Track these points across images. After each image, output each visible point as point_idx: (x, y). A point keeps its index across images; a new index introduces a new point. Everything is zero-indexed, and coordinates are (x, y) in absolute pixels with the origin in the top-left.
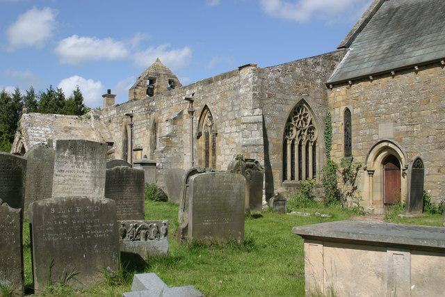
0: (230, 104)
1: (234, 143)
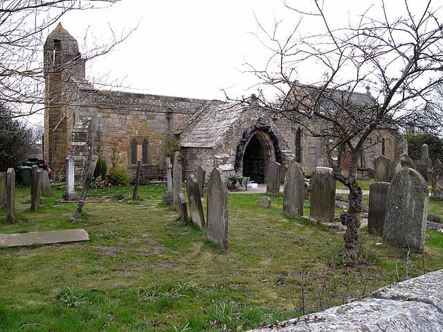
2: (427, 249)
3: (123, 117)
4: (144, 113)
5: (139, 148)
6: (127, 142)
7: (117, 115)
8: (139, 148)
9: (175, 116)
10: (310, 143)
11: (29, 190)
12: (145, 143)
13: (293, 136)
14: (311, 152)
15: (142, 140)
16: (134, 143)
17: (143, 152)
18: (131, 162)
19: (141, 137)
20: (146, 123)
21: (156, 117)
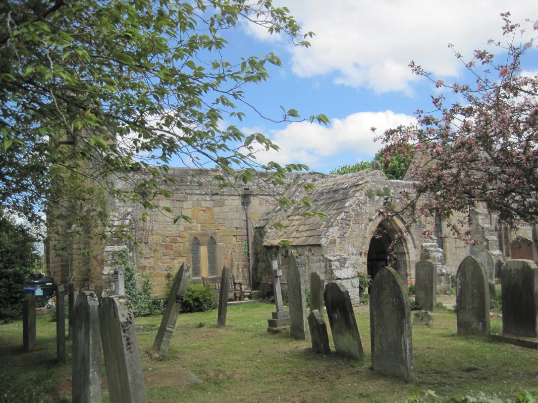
4: (208, 198)
5: (204, 251)
6: (185, 244)
8: (204, 251)
12: (212, 242)
16: (196, 243)
21: (226, 203)
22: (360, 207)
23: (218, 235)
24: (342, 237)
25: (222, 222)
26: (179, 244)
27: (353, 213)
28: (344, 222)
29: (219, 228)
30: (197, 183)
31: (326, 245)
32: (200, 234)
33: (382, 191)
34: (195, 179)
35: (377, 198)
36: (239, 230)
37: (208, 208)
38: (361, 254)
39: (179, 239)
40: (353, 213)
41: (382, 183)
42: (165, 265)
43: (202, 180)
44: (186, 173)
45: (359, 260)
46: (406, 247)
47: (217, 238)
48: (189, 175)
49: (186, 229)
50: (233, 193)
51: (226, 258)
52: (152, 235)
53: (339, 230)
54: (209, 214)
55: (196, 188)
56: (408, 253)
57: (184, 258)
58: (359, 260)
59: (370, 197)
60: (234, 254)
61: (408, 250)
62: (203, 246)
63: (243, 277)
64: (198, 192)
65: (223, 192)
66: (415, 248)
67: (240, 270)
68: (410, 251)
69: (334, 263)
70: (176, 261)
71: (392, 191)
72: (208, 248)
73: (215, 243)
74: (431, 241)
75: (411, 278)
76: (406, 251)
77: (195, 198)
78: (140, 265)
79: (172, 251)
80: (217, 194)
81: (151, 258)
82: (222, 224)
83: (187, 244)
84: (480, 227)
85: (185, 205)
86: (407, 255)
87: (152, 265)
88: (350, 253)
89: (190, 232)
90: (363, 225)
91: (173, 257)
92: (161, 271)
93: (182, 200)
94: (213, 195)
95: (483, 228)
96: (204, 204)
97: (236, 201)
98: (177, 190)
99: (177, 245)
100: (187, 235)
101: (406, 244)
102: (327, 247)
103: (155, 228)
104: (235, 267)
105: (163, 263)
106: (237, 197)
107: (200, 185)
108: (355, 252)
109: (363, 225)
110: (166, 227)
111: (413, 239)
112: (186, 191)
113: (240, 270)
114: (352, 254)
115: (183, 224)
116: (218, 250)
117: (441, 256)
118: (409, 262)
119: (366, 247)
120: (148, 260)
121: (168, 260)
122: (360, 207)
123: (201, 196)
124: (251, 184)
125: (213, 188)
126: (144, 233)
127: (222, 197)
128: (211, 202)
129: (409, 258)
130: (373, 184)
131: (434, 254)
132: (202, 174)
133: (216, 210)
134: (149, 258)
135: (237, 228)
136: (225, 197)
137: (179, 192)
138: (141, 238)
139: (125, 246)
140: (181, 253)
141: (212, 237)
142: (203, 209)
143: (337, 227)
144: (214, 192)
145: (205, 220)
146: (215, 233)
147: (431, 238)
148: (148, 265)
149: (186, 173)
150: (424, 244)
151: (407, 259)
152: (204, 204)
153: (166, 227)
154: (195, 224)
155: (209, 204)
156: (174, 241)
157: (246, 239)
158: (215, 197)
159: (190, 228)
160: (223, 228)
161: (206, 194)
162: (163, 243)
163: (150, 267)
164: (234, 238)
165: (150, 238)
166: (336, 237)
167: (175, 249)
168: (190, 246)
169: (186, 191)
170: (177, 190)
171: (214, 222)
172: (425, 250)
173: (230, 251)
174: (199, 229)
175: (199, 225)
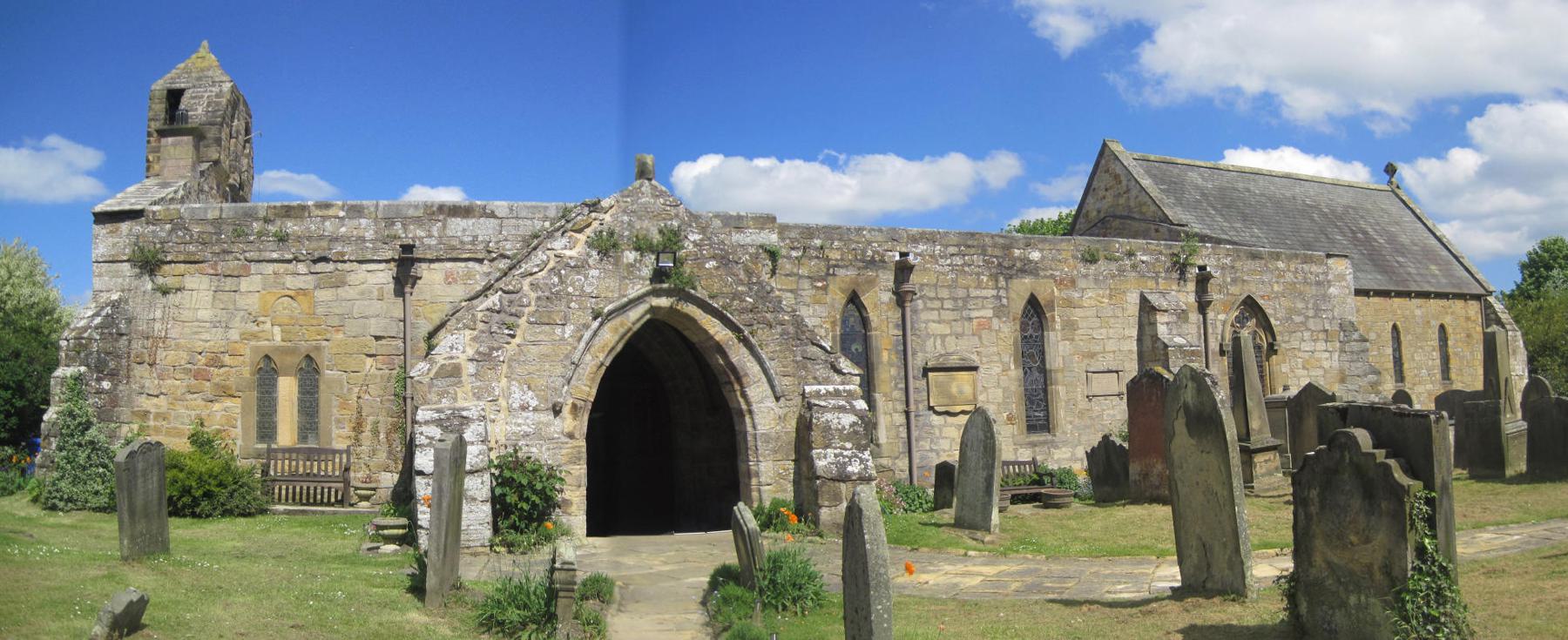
0: (1310, 306)
1: (1321, 367)
2: (639, 182)
3: (229, 283)
4: (302, 268)
5: (287, 388)
6: (242, 370)
7: (206, 279)
8: (287, 388)
9: (431, 277)
10: (1092, 355)
11: (953, 521)
12: (309, 374)
13: (1007, 332)
14: (1096, 390)
15: (296, 360)
16: (267, 374)
17: (301, 401)
18: (254, 433)
19: (292, 351)
20: (314, 305)
21: (351, 278)
22: (560, 276)
23: (326, 354)
24: (484, 359)
25: (336, 322)
26: (227, 369)
27: (533, 295)
28: (496, 317)
29: (328, 336)
30: (275, 235)
31: (426, 380)
32: (277, 349)
33: (656, 238)
34: (270, 227)
35: (630, 256)
36: (383, 342)
37: (302, 291)
38: (556, 410)
39: (227, 359)
40: (533, 295)
41: (656, 216)
42: (193, 413)
43: (291, 227)
44: (251, 216)
45: (548, 425)
46: (744, 395)
47: (324, 360)
48: (257, 219)
49: (246, 337)
50: (369, 257)
51: (344, 406)
52: (165, 349)
53: (474, 339)
54: (305, 306)
55: (272, 246)
56: (750, 412)
57: (239, 400)
58: (548, 425)
59: (604, 253)
60: (367, 397)
61: (748, 403)
62: (286, 375)
63: (390, 453)
64: (275, 255)
65: (343, 254)
66: (777, 399)
67: (382, 436)
68: (755, 407)
69: (424, 429)
70: (217, 406)
71: (693, 237)
72: (300, 380)
73: (317, 371)
74: (837, 378)
75: (760, 484)
76: (744, 407)
77: (269, 268)
78: (136, 409)
79: (208, 384)
80: (324, 259)
81: (162, 396)
82: (338, 328)
83: (246, 372)
84: (1159, 344)
85: (245, 284)
86: (748, 419)
87: (163, 410)
88: (516, 405)
89: (253, 343)
90: (569, 330)
91: (211, 397)
92: (183, 423)
93: (236, 273)
94: (315, 262)
95: (1166, 346)
96: (290, 282)
97: (381, 274)
98: (225, 252)
99: (223, 370)
100: (248, 351)
101: (742, 387)
102: (431, 386)
103: (173, 333)
104: (368, 427)
105: (187, 408)
106: (382, 266)
107: (282, 239)
108: (534, 403)
109: (569, 330)
110: (196, 333)
111: (765, 371)
112: (247, 255)
113: (382, 436)
114: (524, 408)
115: (237, 325)
116: (322, 387)
117: (853, 424)
118: (755, 436)
119: (586, 388)
120: (155, 400)
121: (200, 402)
122: (560, 276)
123: (286, 265)
124: (423, 234)
125: (314, 245)
126: (149, 343)
127: (340, 266)
128: (310, 277)
129: (754, 427)
130: (626, 218)
131: (829, 416)
132: (289, 216)
133: (324, 295)
134: (157, 396)
135: (378, 338)
136: (347, 266)
137: (231, 257)
138: (142, 353)
139: (83, 369)
140: (230, 388)
141: (308, 357)
142: (289, 293)
143: (468, 332)
144: (317, 255)
145: (291, 318)
146: (318, 348)
147: (839, 372)
148: (153, 410)
149: (251, 216)
150: (808, 389)
151: (749, 429)
152: (290, 282)
153: (196, 333)
154: (268, 326)
155: (307, 282)
156: (215, 362)
157: (402, 363)
158: (320, 267)
159: (255, 336)
160: (340, 336)
161: (296, 259)
162: (189, 366)
163: (158, 416)
164: (369, 361)
165: (161, 354)
166: (462, 359)
167: (217, 380)
168: (253, 374)
169: (247, 255)
170: (225, 252)
171: (314, 322)
172: (809, 403)
173: (356, 390)
174: (278, 338)
175: (277, 330)
